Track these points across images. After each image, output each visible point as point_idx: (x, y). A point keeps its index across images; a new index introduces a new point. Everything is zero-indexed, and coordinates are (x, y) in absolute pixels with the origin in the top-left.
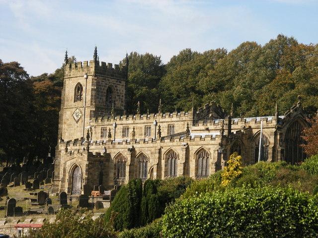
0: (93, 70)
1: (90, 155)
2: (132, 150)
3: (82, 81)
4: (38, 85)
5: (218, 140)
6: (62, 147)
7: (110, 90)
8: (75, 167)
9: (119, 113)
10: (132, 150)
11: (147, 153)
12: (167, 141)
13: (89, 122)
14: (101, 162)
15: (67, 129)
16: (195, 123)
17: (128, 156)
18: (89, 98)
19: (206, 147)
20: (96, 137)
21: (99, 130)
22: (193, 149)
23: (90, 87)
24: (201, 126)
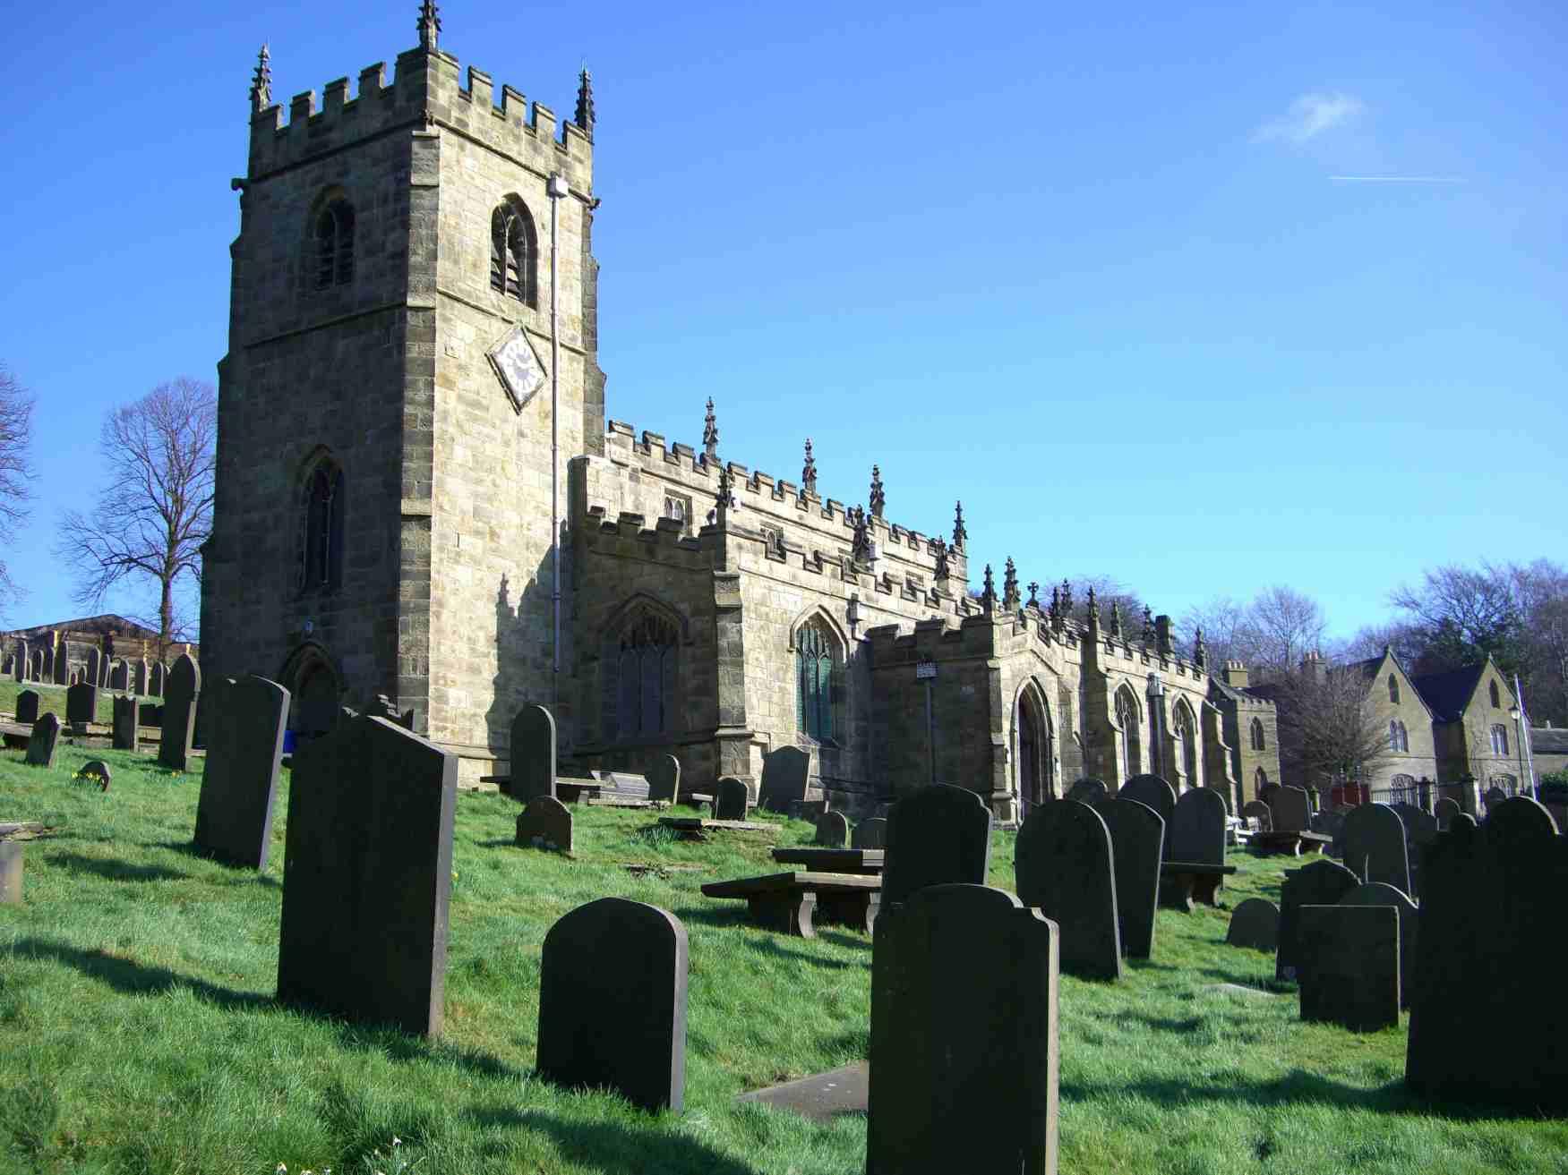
15: (459, 425)
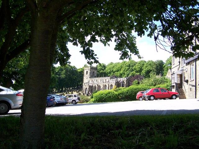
0: (90, 68)
1: (89, 86)
2: (98, 85)
3: (88, 70)
4: (79, 71)
5: (115, 83)
6: (83, 84)
7: (93, 72)
8: (86, 88)
9: (95, 77)
10: (98, 85)
11: (101, 85)
12: (105, 83)
13: (89, 79)
14: (91, 87)
16: (110, 79)
17: (97, 86)
18: (89, 74)
19: (112, 84)
20: (91, 82)
21: (91, 80)
22: (110, 85)
23: (89, 72)
24: (112, 80)
